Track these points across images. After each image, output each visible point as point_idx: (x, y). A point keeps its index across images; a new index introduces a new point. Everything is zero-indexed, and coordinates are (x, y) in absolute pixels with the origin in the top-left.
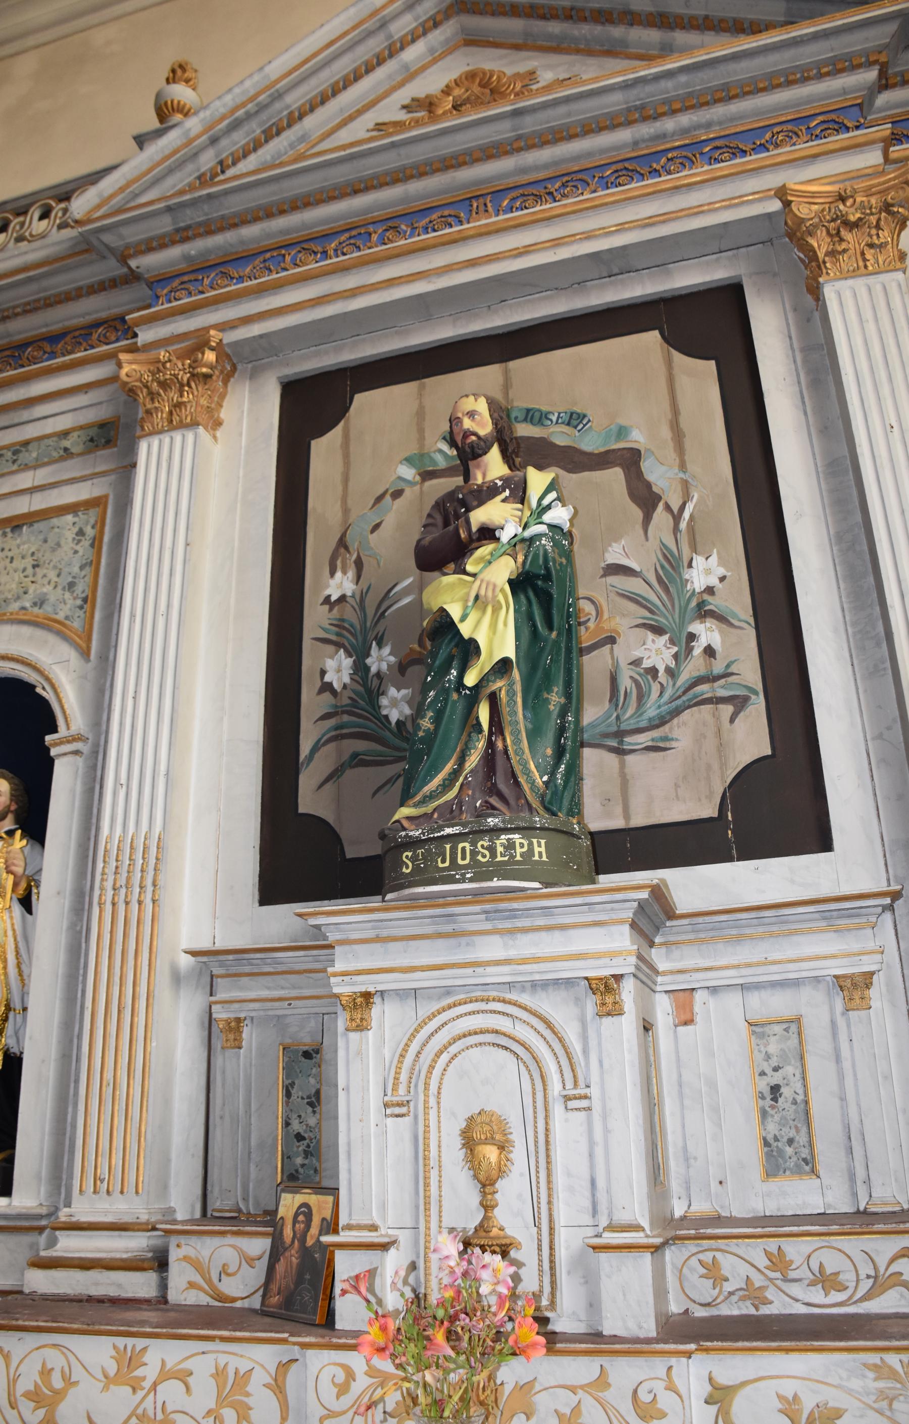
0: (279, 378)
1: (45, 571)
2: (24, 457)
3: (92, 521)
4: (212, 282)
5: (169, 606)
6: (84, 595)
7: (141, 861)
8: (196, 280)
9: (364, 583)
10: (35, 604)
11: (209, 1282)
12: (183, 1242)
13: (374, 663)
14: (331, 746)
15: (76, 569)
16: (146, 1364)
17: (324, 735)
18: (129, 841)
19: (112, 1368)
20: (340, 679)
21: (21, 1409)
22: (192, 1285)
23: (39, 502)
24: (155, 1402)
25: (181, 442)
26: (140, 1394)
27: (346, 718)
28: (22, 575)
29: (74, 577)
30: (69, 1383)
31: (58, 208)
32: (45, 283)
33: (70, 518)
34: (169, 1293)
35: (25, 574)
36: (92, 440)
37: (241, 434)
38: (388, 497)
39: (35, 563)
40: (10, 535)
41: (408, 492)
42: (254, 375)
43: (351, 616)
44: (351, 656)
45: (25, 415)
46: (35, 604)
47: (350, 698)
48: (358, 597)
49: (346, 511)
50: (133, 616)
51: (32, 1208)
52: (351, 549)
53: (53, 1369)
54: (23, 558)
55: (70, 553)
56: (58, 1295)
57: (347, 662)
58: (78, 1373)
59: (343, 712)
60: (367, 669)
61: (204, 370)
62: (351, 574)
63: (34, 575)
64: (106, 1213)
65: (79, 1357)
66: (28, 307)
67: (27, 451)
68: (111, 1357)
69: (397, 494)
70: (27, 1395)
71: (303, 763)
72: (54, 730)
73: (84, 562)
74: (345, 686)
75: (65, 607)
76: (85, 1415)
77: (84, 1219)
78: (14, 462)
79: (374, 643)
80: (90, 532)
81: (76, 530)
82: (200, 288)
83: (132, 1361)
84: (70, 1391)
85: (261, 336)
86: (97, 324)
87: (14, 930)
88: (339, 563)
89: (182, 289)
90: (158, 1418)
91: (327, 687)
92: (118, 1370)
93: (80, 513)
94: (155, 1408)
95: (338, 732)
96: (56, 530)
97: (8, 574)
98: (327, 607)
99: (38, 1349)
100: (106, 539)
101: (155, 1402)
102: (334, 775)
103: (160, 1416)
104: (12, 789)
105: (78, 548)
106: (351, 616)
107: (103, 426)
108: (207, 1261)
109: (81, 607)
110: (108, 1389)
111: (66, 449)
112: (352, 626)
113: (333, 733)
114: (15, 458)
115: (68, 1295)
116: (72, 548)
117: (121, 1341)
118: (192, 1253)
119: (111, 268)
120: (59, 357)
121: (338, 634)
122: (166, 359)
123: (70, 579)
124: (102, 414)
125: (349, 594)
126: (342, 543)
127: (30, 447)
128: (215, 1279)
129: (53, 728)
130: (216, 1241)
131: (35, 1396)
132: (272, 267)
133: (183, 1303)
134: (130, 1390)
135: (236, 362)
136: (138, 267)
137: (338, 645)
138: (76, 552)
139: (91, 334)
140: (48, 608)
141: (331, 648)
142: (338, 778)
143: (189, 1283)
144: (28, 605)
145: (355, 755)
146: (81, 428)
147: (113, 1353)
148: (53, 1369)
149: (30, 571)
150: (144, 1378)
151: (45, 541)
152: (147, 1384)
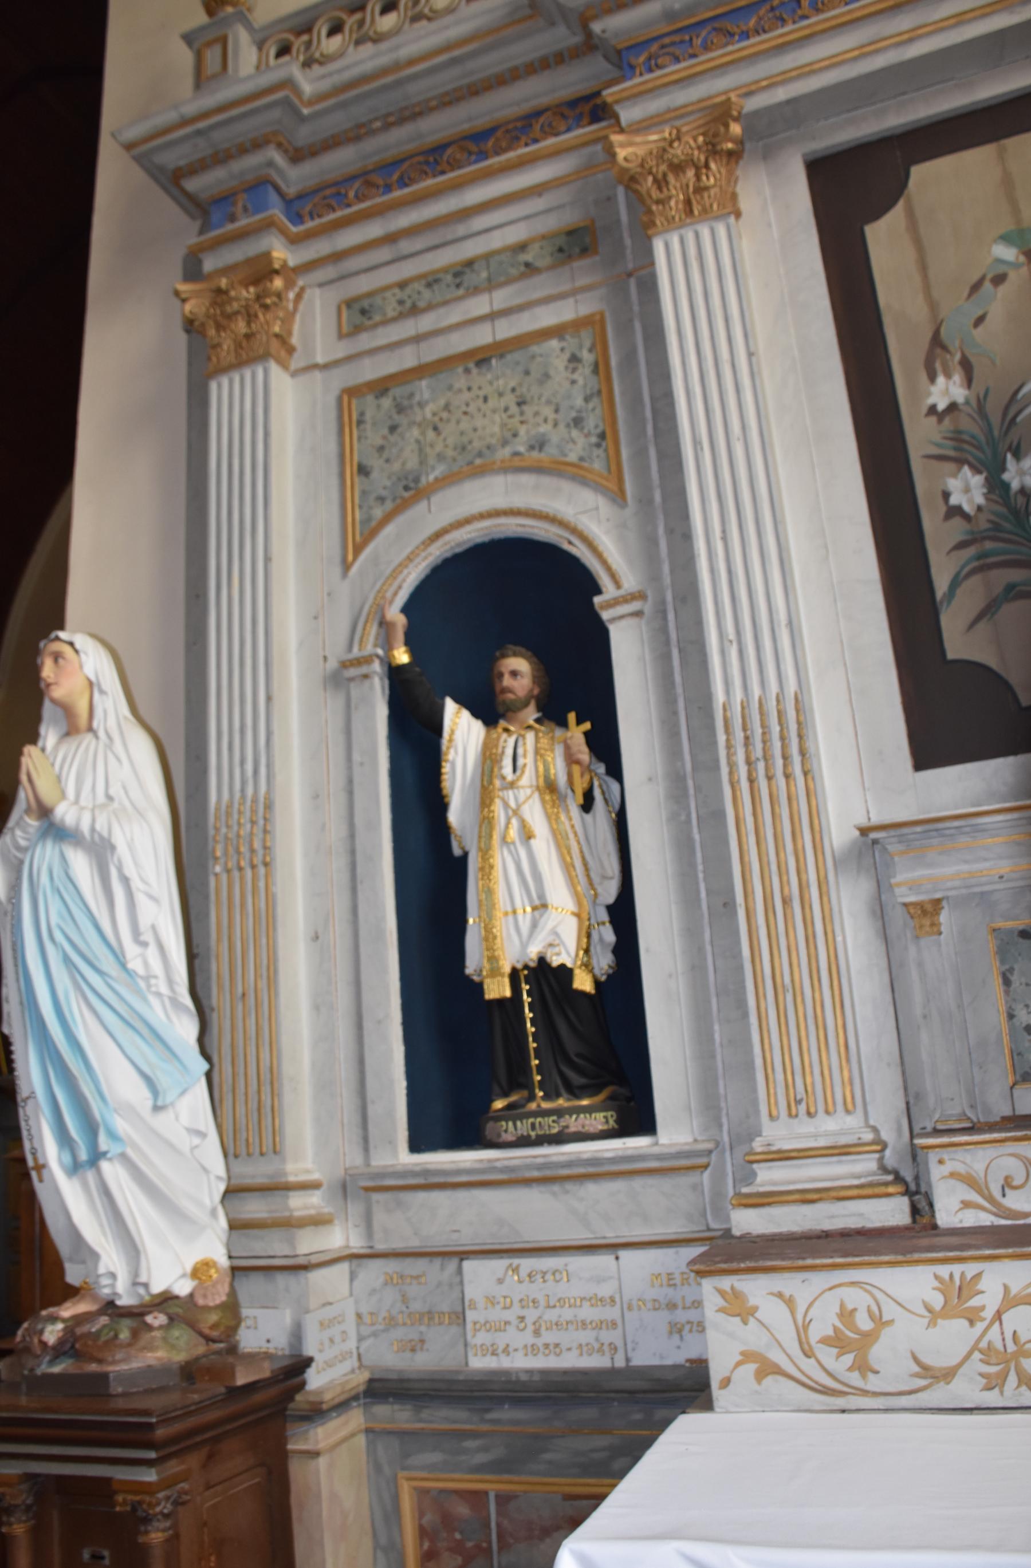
0: (804, 156)
1: (536, 408)
2: (471, 279)
3: (587, 343)
4: (705, 41)
5: (744, 427)
6: (599, 430)
7: (778, 728)
8: (682, 42)
9: (978, 386)
10: (532, 448)
11: (991, 1199)
12: (945, 1157)
13: (1013, 478)
14: (976, 579)
15: (579, 402)
16: (983, 1292)
17: (963, 567)
18: (757, 705)
19: (937, 1301)
20: (970, 501)
21: (820, 1356)
22: (966, 1205)
23: (506, 329)
24: (1002, 1333)
25: (710, 235)
26: (980, 1326)
27: (989, 545)
28: (504, 416)
29: (579, 411)
30: (880, 1322)
31: (298, 43)
32: (471, 65)
33: (554, 343)
34: (938, 1215)
35: (509, 413)
36: (561, 250)
37: (769, 225)
38: (987, 285)
39: (520, 400)
40: (475, 371)
41: (1012, 275)
42: (767, 155)
43: (968, 425)
44: (979, 472)
45: (461, 230)
46: (532, 448)
47: (989, 521)
48: (974, 404)
49: (933, 306)
50: (697, 443)
51: (686, 1144)
52: (951, 348)
53: (855, 1310)
54: (501, 395)
55: (567, 384)
56: (781, 1234)
57: (977, 481)
58: (890, 1311)
59: (984, 538)
60: (1006, 486)
61: (730, 145)
62: (957, 377)
63: (522, 413)
64: (816, 1136)
65: (889, 1292)
66: (447, 99)
67: (473, 271)
68: (934, 1289)
69: (999, 279)
70: (825, 1341)
71: (941, 602)
72: (598, 591)
73: (588, 392)
74: (979, 508)
75: (578, 446)
76: (909, 1355)
77: (787, 1146)
78: (458, 286)
79: (1009, 456)
80: (587, 357)
81: (567, 355)
82: (691, 51)
83: (966, 1289)
84: (883, 1332)
85: (788, 102)
86: (538, 113)
87: (576, 834)
88: (938, 365)
89: (664, 54)
90: (1009, 1350)
91: (956, 511)
92: (946, 1302)
93: (568, 337)
94: (1004, 1340)
95: (982, 562)
96: (539, 359)
97: (484, 416)
98: (933, 419)
99: (831, 1289)
100: (614, 362)
101: (1002, 1333)
102: (988, 611)
103: (1011, 1347)
104: (533, 669)
105: (575, 376)
106: (968, 425)
107: (571, 233)
108: (982, 1175)
109: (598, 445)
110: (935, 1325)
111: (527, 265)
112: (973, 437)
113: (975, 564)
114: (458, 280)
115: (793, 1233)
116: (567, 378)
117: (944, 1270)
118: (961, 1168)
119: (562, 37)
120: (492, 157)
121: (955, 449)
122: (674, 136)
123: (574, 414)
124: (569, 218)
125: (960, 400)
126: (937, 342)
127: (476, 266)
128: (997, 1193)
129: (597, 589)
130: (991, 1152)
131: (837, 1341)
132: (785, 16)
133: (960, 1225)
134: (966, 1323)
135: (767, 132)
136: (604, 31)
137: (960, 462)
138: (574, 382)
139: (531, 125)
140: (552, 450)
141: (950, 466)
142: (993, 615)
143: (962, 1202)
144: (522, 449)
145: (1010, 588)
146: (543, 237)
147: (937, 1284)
148: (855, 1310)
149: (514, 409)
150: (983, 1308)
151: (527, 373)
152: (989, 1314)
